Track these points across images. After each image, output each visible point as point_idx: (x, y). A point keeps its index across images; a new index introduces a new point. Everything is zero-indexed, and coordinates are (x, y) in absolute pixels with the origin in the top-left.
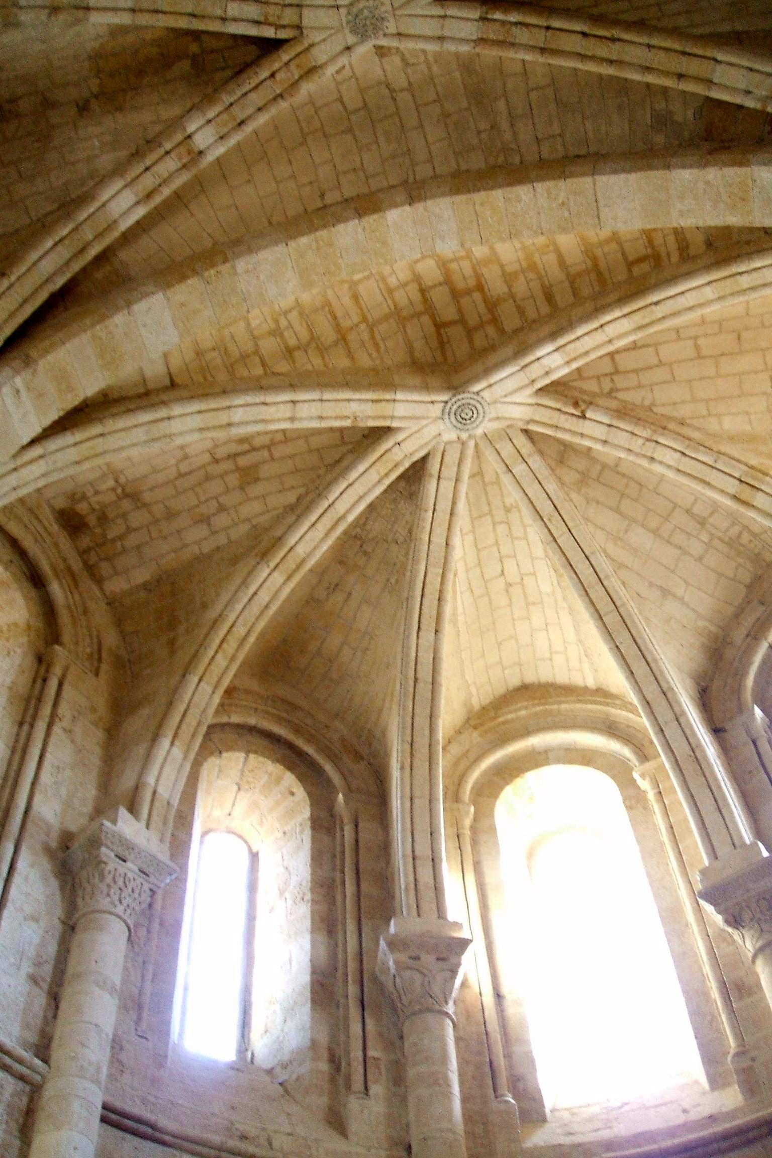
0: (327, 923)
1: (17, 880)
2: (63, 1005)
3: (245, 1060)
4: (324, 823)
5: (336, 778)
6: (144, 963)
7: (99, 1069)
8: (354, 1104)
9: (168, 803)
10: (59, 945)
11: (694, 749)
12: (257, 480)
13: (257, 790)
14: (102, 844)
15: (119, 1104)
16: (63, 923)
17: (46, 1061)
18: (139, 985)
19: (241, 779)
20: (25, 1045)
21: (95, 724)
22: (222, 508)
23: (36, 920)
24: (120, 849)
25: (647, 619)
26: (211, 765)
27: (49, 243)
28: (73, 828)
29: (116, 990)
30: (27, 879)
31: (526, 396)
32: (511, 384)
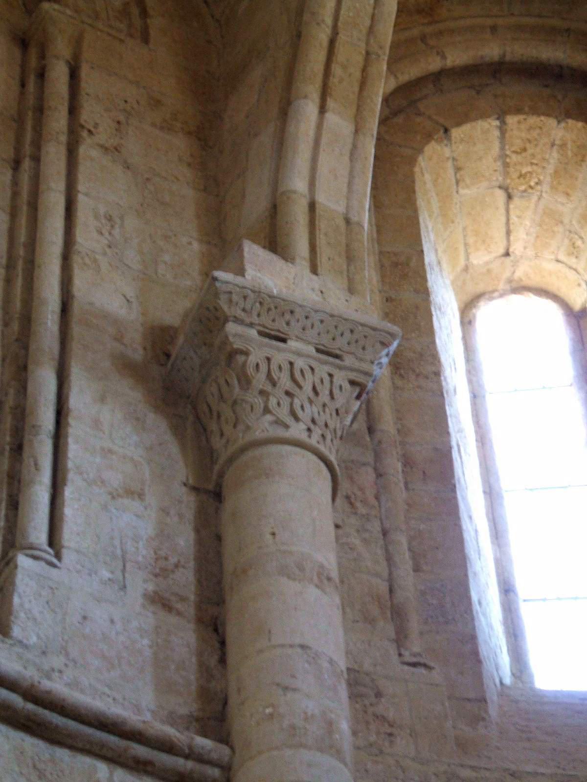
1: (75, 430)
2: (232, 632)
6: (385, 533)
7: (330, 726)
9: (348, 221)
10: (197, 531)
13: (545, 187)
14: (226, 320)
16: (195, 489)
17: (224, 739)
18: (385, 574)
19: (506, 174)
20: (172, 719)
21: (166, 127)
24: (266, 320)
26: (432, 165)
29: (329, 579)
30: (96, 424)
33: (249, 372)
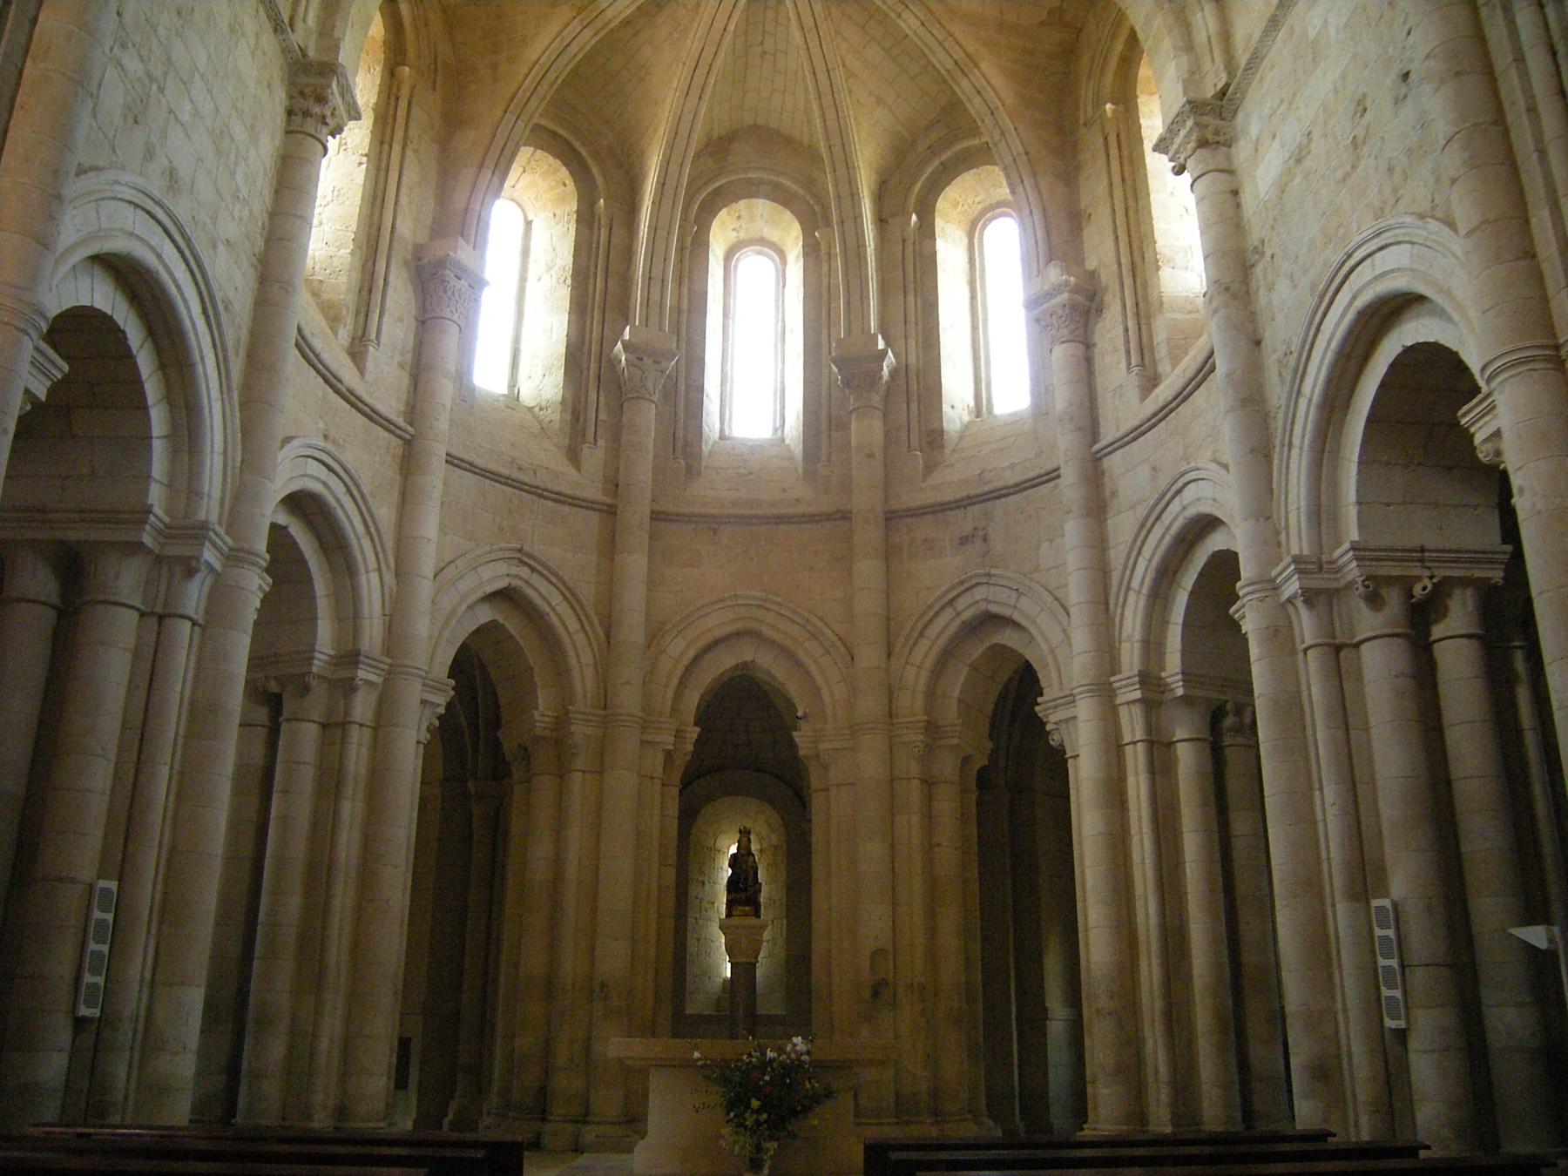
0: (580, 307)
1: (390, 292)
3: (513, 398)
4: (586, 219)
5: (599, 180)
8: (586, 450)
11: (861, 246)
15: (453, 452)
23: (401, 320)
25: (858, 124)
28: (420, 240)
33: (541, 851)
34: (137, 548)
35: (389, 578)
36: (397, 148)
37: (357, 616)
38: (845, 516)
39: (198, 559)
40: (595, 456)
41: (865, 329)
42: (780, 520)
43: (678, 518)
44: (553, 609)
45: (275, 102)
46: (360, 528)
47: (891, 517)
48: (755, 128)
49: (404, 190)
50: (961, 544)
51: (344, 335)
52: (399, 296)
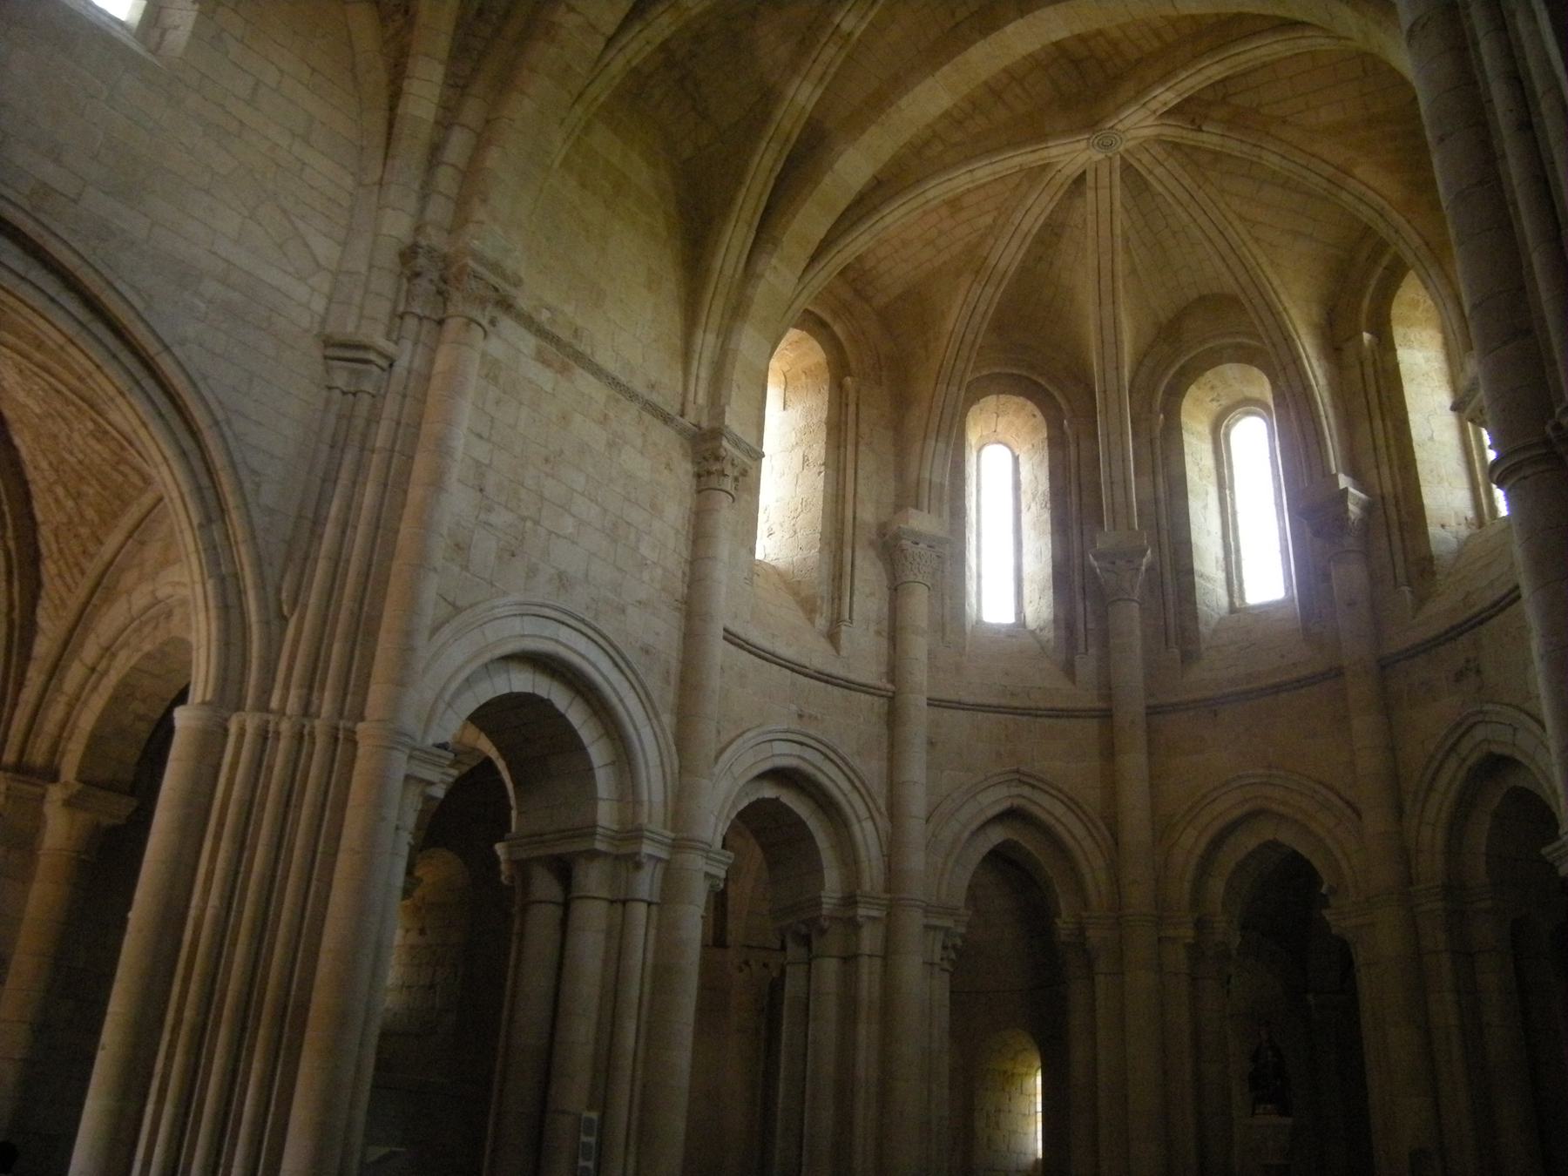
1: (857, 573)
3: (1021, 622)
4: (1057, 444)
5: (1064, 405)
12: (962, 208)
22: (941, 233)
27: (764, 145)
31: (1150, 121)
32: (1135, 118)
34: (593, 854)
35: (883, 823)
36: (850, 448)
37: (856, 862)
38: (1338, 672)
39: (638, 853)
40: (1087, 666)
41: (1130, 527)
42: (1277, 689)
43: (1175, 707)
44: (1058, 820)
45: (684, 469)
46: (846, 786)
47: (1152, 711)
48: (1202, 299)
49: (860, 481)
50: (1457, 681)
51: (821, 622)
52: (868, 574)
